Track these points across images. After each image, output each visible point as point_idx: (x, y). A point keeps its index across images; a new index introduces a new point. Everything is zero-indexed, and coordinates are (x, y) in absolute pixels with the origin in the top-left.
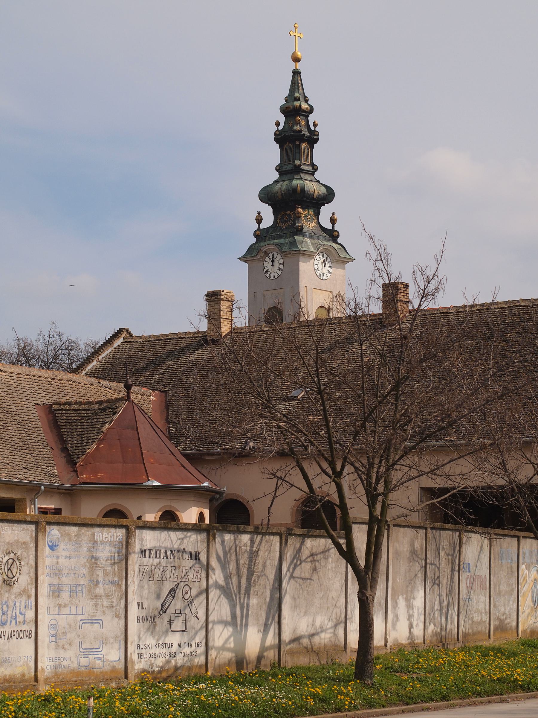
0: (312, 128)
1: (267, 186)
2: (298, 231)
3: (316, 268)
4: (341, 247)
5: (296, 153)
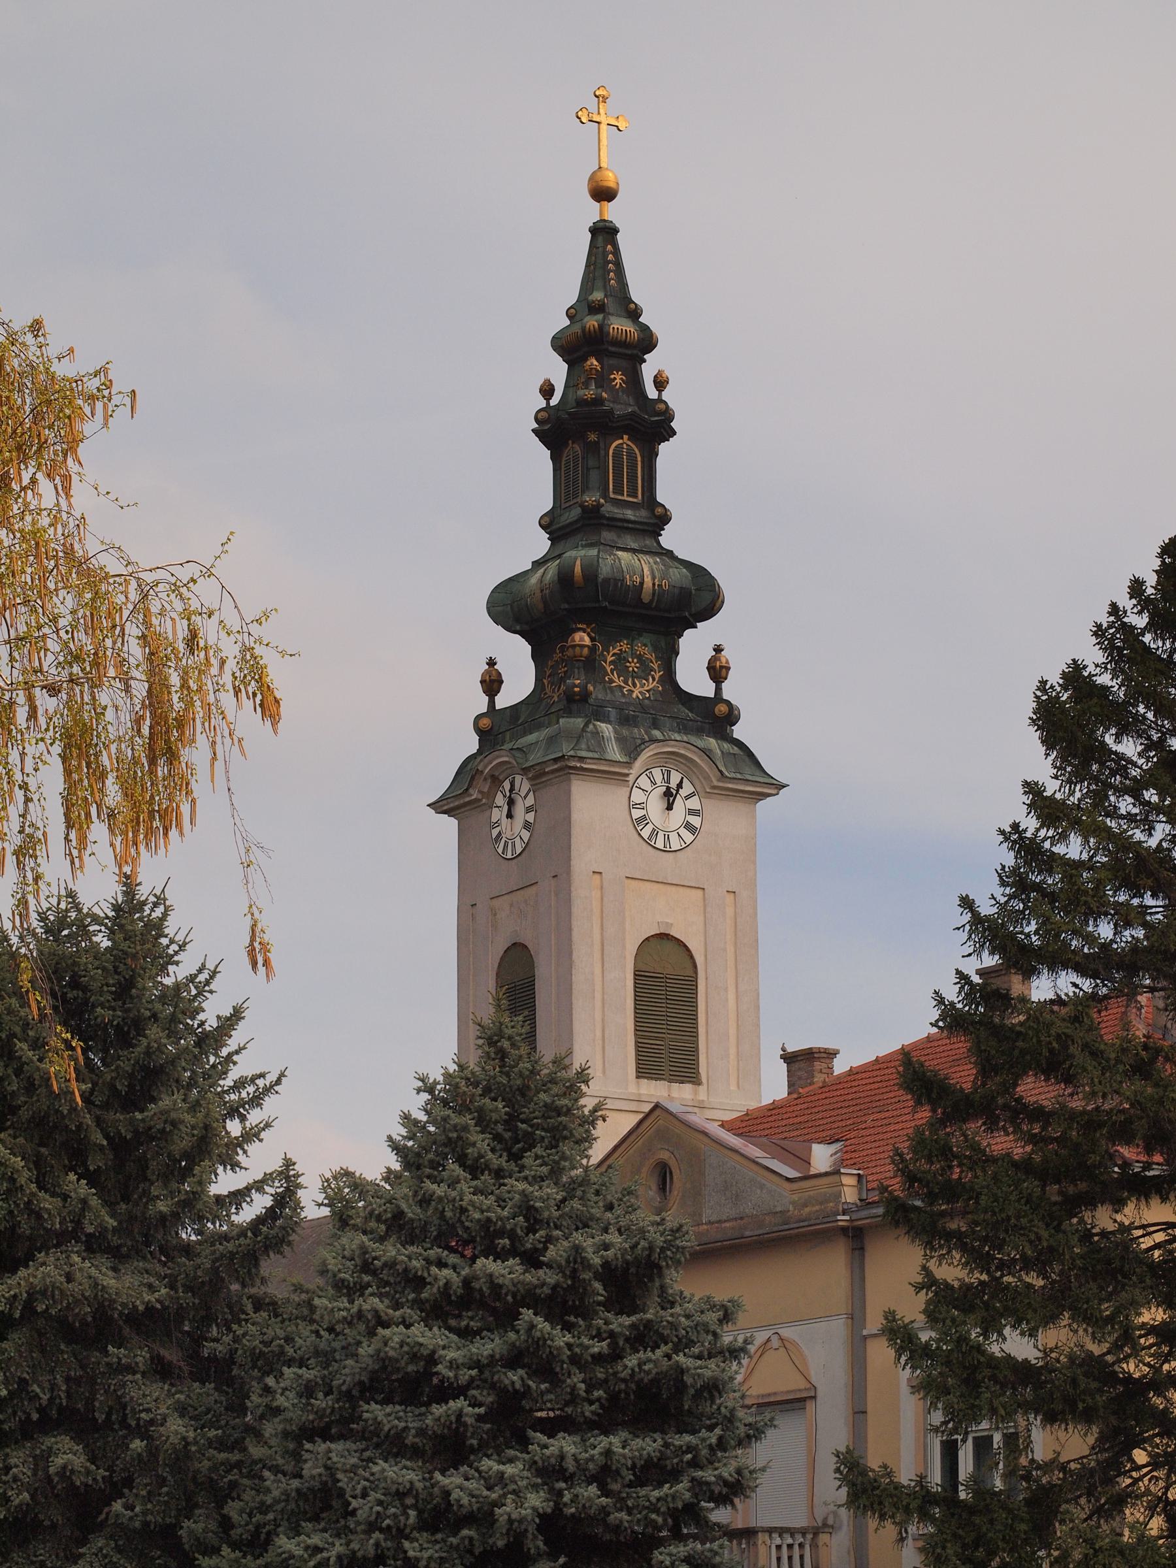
0: (652, 393)
1: (510, 579)
2: (574, 701)
3: (637, 814)
4: (736, 750)
5: (588, 469)
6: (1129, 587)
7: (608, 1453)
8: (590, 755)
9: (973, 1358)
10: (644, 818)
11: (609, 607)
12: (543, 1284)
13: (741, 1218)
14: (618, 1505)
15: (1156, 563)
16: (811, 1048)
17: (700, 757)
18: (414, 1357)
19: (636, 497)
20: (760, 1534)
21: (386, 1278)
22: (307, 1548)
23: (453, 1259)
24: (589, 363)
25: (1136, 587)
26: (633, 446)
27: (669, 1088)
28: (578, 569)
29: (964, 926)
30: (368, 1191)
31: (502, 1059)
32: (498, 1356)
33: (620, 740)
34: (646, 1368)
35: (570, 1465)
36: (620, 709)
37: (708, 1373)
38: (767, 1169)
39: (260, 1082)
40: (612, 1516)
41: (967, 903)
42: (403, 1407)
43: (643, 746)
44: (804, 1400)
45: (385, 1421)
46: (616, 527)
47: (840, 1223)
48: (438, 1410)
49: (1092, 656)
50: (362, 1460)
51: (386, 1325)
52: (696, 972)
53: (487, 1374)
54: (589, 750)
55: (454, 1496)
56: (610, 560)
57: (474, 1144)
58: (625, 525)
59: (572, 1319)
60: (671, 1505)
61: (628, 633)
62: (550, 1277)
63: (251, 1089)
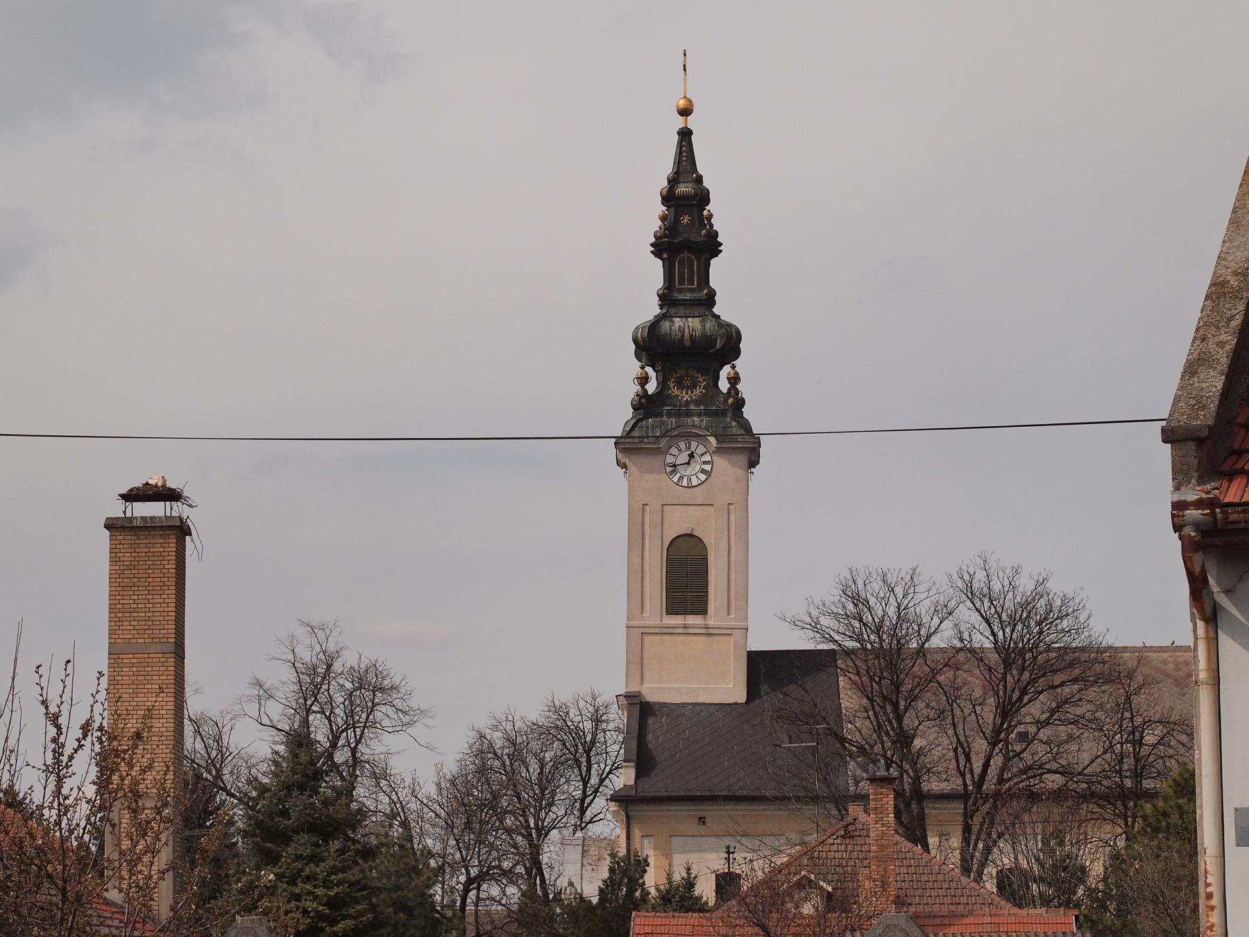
6: (652, 245)
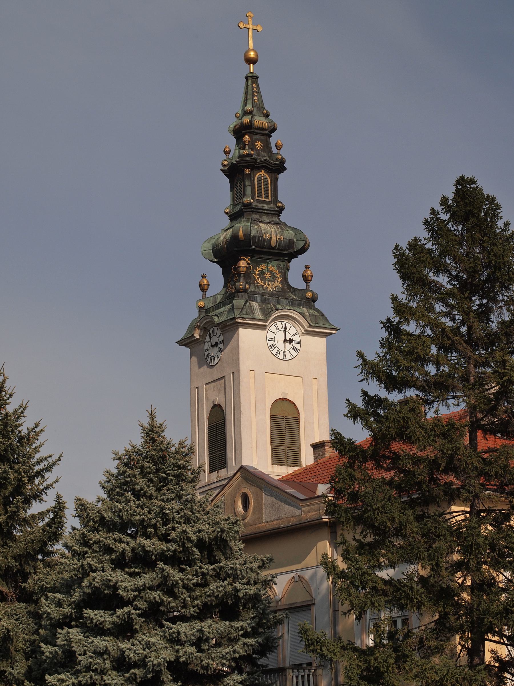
0: (275, 151)
3: (270, 343)
4: (316, 313)
7: (201, 631)
8: (248, 316)
9: (365, 578)
10: (273, 345)
11: (256, 249)
12: (169, 550)
13: (280, 519)
14: (207, 657)
15: (454, 189)
16: (324, 441)
17: (299, 317)
18: (108, 587)
19: (268, 198)
20: (287, 670)
21: (95, 549)
22: (58, 680)
23: (127, 539)
24: (245, 138)
25: (444, 201)
26: (267, 175)
27: (287, 469)
28: (241, 232)
29: (359, 366)
30: (88, 507)
31: (153, 443)
32: (147, 585)
33: (262, 310)
34: (220, 589)
35: (183, 637)
36: (262, 295)
37: (252, 592)
38: (292, 495)
39: (50, 460)
40: (204, 662)
41: (360, 355)
42: (103, 611)
43: (272, 312)
44: (309, 605)
45: (94, 618)
46: (259, 212)
47: (324, 520)
48: (119, 612)
49: (423, 234)
50: (85, 637)
51: (94, 571)
52: (299, 416)
53: (143, 594)
54: (247, 314)
55: (126, 653)
56: (256, 227)
57: (138, 484)
58: (264, 211)
59: (184, 566)
60: (233, 656)
61: (264, 261)
62: (173, 547)
63: (46, 463)
